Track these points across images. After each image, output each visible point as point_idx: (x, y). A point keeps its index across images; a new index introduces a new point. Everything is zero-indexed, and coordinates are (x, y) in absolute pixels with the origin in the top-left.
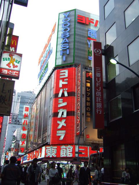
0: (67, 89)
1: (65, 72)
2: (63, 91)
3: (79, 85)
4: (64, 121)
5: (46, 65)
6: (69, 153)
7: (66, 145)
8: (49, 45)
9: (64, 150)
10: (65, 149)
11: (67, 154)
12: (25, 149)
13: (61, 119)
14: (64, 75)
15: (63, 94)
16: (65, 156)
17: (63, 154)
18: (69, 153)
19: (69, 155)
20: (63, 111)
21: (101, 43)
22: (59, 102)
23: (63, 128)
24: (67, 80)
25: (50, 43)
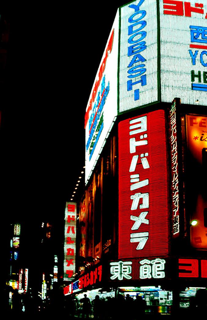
0: (147, 154)
1: (140, 122)
2: (140, 159)
3: (175, 143)
4: (144, 215)
5: (99, 121)
6: (158, 271)
7: (151, 258)
8: (101, 82)
9: (147, 266)
10: (150, 266)
11: (153, 274)
12: (74, 272)
13: (137, 213)
14: (140, 128)
15: (139, 164)
16: (150, 277)
17: (144, 274)
18: (158, 271)
19: (159, 275)
20: (141, 197)
21: (142, 223)
22: (132, 181)
23: (143, 228)
24: (146, 136)
25: (103, 76)
